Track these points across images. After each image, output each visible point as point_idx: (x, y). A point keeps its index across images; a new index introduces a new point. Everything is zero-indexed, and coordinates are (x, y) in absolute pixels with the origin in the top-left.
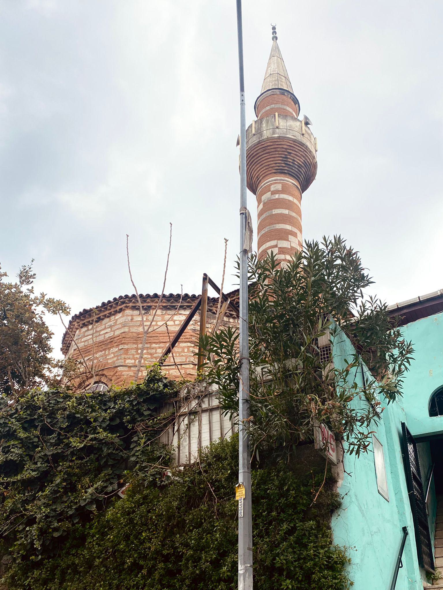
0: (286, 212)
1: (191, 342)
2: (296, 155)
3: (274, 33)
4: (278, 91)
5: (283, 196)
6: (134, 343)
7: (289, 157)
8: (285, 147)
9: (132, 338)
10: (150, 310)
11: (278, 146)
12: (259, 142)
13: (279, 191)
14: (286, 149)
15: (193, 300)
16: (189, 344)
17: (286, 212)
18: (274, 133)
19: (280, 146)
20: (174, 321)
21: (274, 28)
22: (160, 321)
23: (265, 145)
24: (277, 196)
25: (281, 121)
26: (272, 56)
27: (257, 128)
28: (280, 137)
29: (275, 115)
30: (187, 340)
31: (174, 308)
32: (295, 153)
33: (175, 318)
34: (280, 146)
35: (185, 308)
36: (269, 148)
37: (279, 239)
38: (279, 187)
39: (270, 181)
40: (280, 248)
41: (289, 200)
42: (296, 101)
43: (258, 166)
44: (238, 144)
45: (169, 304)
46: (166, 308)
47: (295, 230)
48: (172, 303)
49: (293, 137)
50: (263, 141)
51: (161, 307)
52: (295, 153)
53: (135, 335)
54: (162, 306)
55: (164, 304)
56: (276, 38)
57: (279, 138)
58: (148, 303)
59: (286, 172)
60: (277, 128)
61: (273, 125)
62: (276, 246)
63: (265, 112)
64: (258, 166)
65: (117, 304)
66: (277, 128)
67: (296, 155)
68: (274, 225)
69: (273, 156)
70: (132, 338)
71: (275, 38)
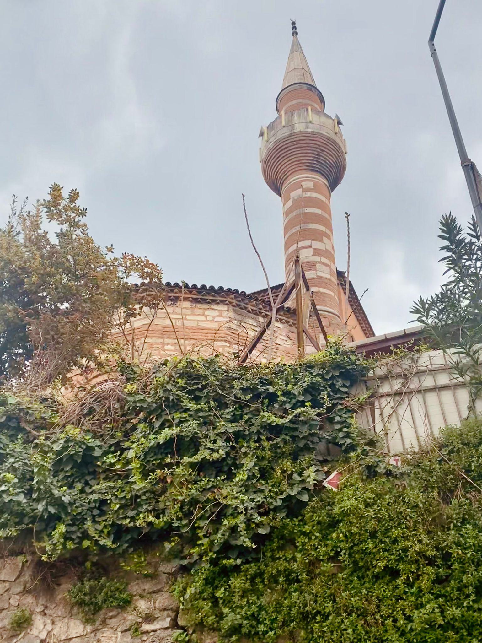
0: (319, 211)
1: (225, 341)
2: (328, 153)
3: (294, 28)
4: (305, 86)
5: (315, 195)
6: (159, 337)
7: (321, 154)
8: (318, 143)
9: (157, 331)
10: (176, 302)
11: (310, 142)
12: (290, 135)
13: (311, 189)
14: (319, 146)
15: (228, 295)
16: (225, 344)
17: (319, 211)
18: (307, 127)
19: (314, 142)
20: (206, 316)
21: (293, 23)
22: (189, 315)
23: (297, 139)
24: (309, 194)
25: (314, 116)
26: (292, 51)
27: (287, 120)
28: (313, 132)
29: (307, 110)
30: (222, 339)
31: (204, 301)
32: (328, 151)
33: (207, 312)
34: (314, 142)
35: (218, 303)
36: (301, 142)
37: (313, 240)
38: (311, 185)
39: (298, 178)
40: (315, 249)
41: (322, 201)
42: (322, 100)
43: (286, 161)
44: (262, 134)
45: (201, 297)
46: (195, 301)
47: (328, 232)
48: (203, 296)
49: (327, 134)
50: (295, 134)
51: (191, 299)
52: (328, 151)
53: (160, 327)
54: (192, 298)
55: (195, 297)
56: (297, 34)
57: (313, 133)
58: (176, 293)
59: (317, 170)
60: (311, 122)
61: (305, 119)
62: (310, 247)
63: (291, 106)
64: (286, 161)
65: (137, 291)
66: (311, 122)
67: (328, 153)
68: (307, 224)
69: (305, 151)
70: (157, 331)
71: (295, 34)
